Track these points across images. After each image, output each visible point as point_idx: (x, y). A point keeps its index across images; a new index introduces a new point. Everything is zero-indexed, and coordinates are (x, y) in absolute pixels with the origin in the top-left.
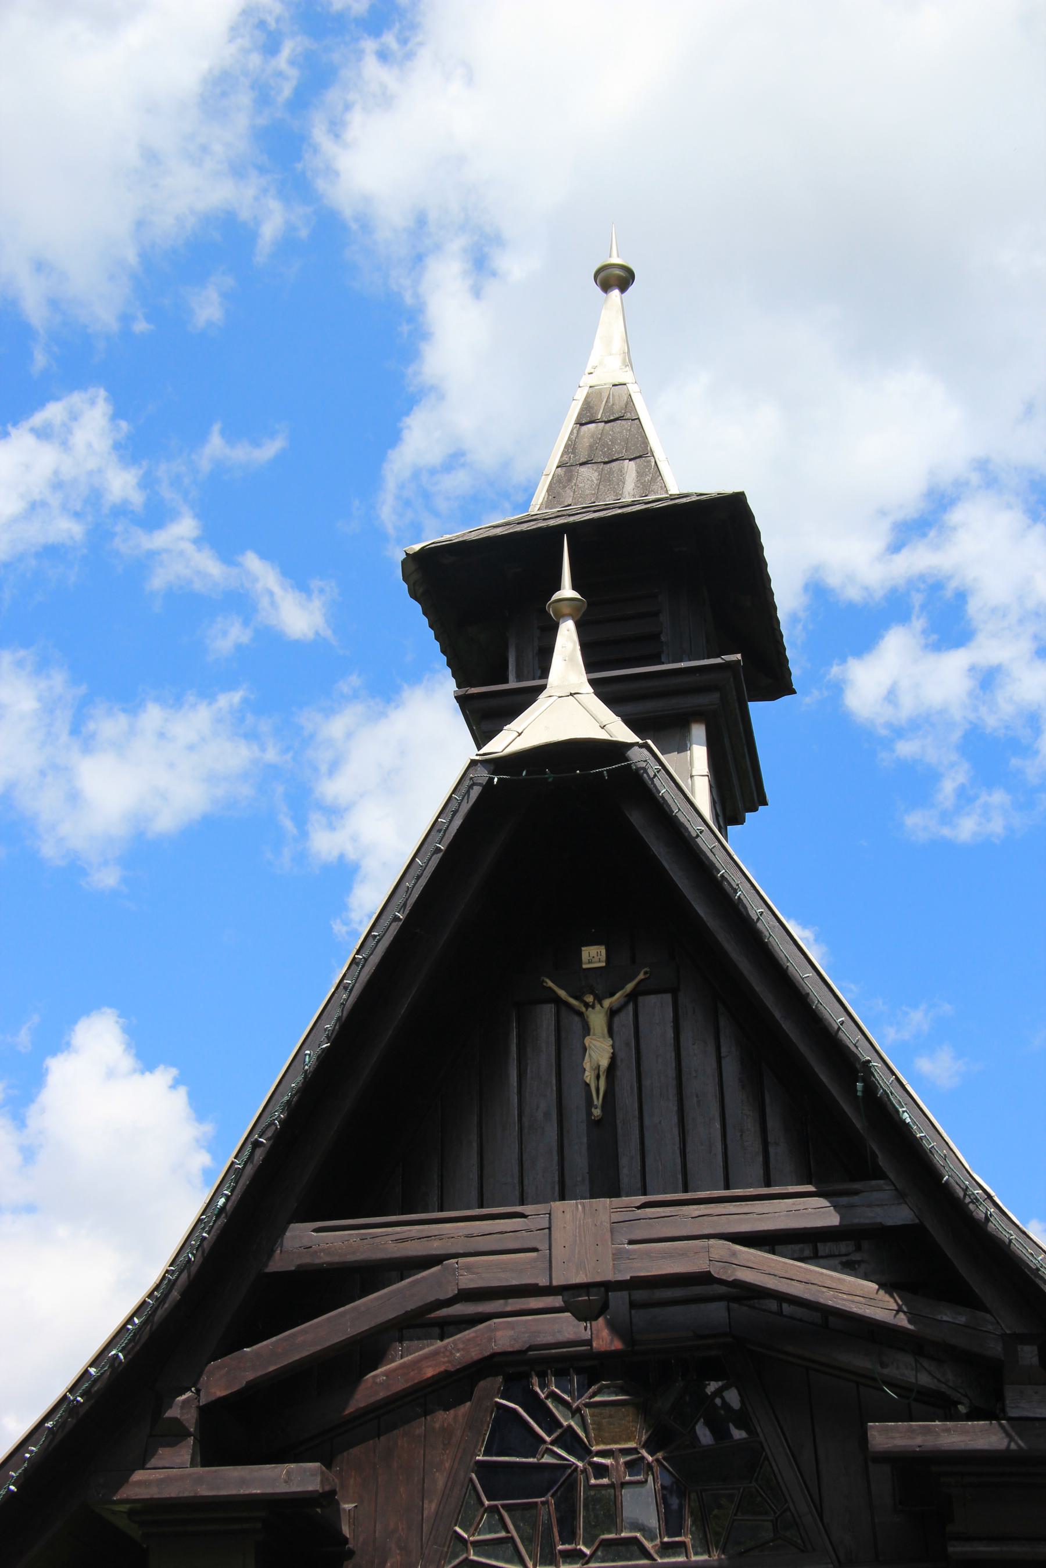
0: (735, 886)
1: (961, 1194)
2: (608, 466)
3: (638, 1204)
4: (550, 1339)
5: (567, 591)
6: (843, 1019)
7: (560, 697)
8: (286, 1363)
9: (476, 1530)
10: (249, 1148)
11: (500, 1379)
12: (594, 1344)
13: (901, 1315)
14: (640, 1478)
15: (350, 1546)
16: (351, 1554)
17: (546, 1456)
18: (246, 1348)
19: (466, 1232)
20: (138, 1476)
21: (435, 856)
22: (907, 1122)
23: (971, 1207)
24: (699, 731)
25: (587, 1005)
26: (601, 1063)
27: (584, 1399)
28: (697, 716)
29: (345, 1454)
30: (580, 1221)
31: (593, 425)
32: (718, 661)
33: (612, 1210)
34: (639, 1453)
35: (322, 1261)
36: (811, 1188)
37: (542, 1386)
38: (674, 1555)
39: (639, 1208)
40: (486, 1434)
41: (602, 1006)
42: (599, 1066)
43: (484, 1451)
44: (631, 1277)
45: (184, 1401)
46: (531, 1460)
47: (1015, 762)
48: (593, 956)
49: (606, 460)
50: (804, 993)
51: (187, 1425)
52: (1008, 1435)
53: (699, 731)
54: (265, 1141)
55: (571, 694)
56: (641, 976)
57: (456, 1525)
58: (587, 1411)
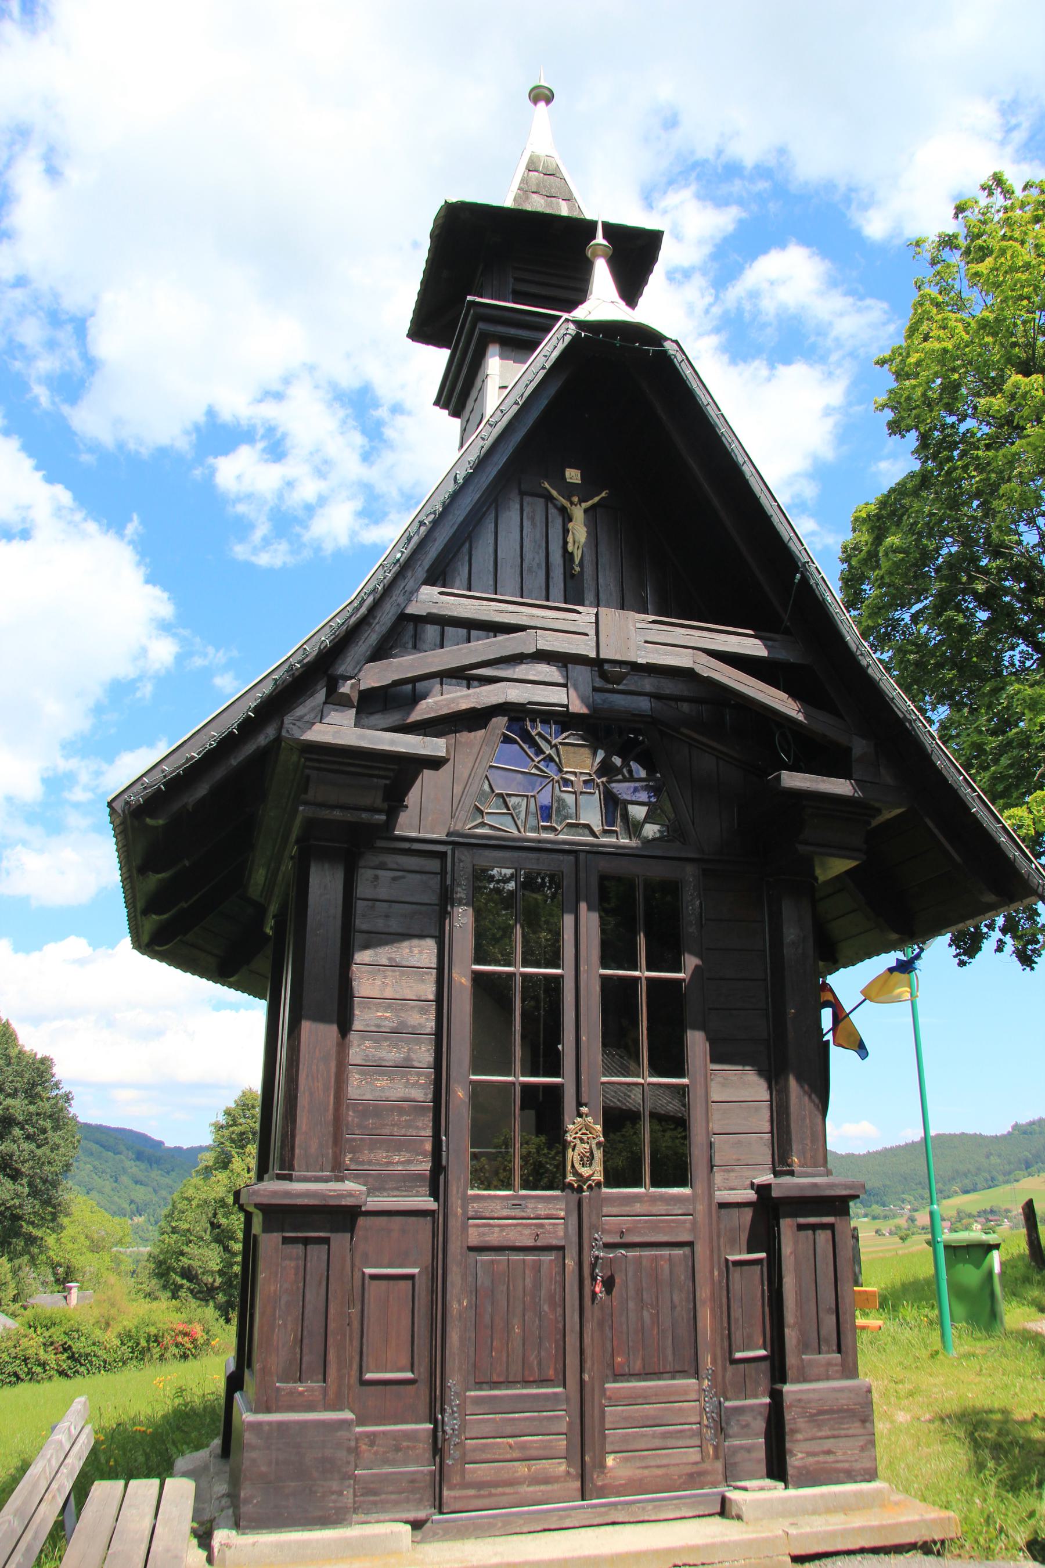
0: (730, 441)
10: (416, 524)
11: (506, 718)
12: (570, 707)
13: (800, 714)
14: (592, 791)
23: (860, 657)
25: (572, 503)
27: (559, 740)
36: (751, 632)
38: (610, 837)
39: (650, 622)
47: (298, 529)
48: (573, 475)
52: (854, 788)
55: (613, 302)
58: (560, 747)
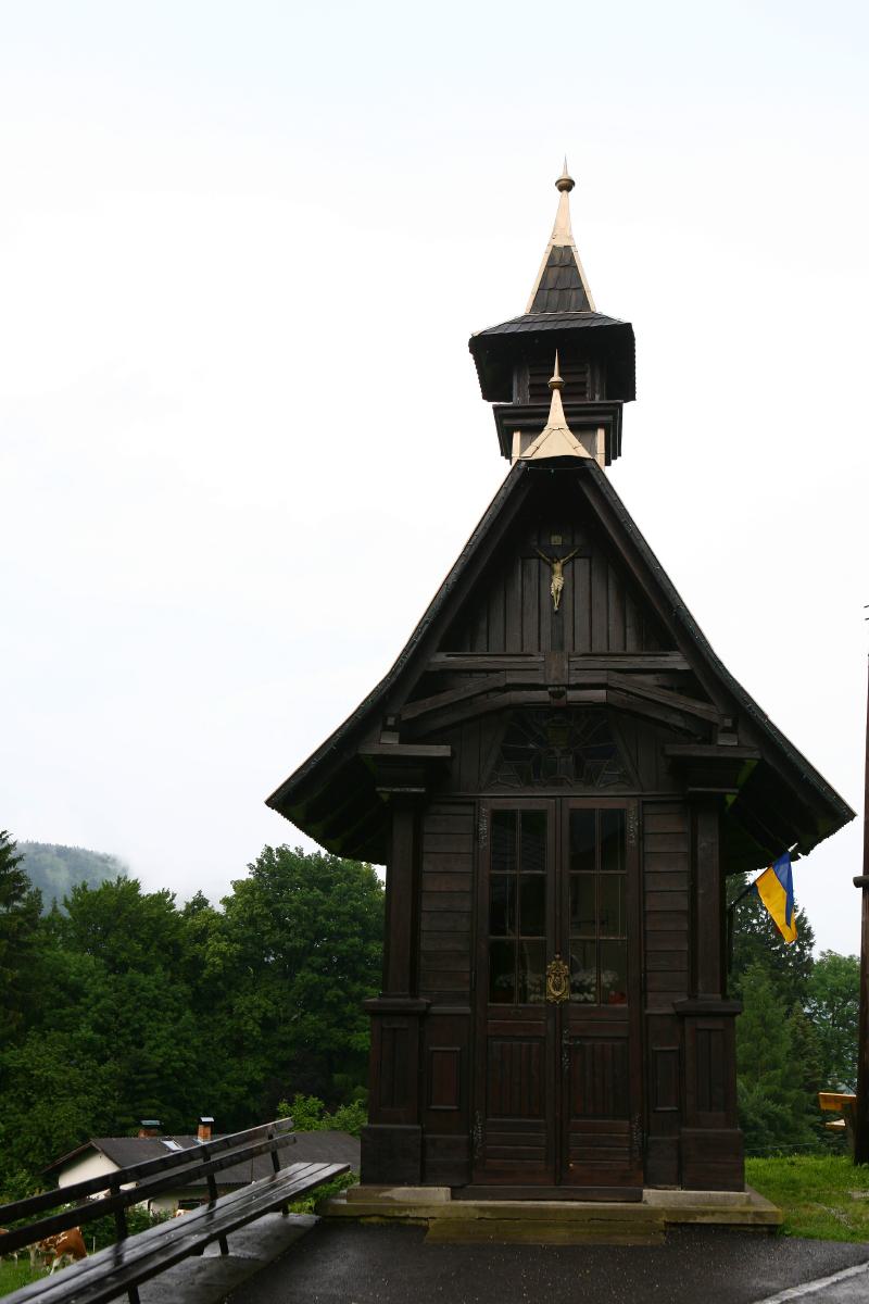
5: (556, 378)
28: (602, 425)
48: (556, 540)
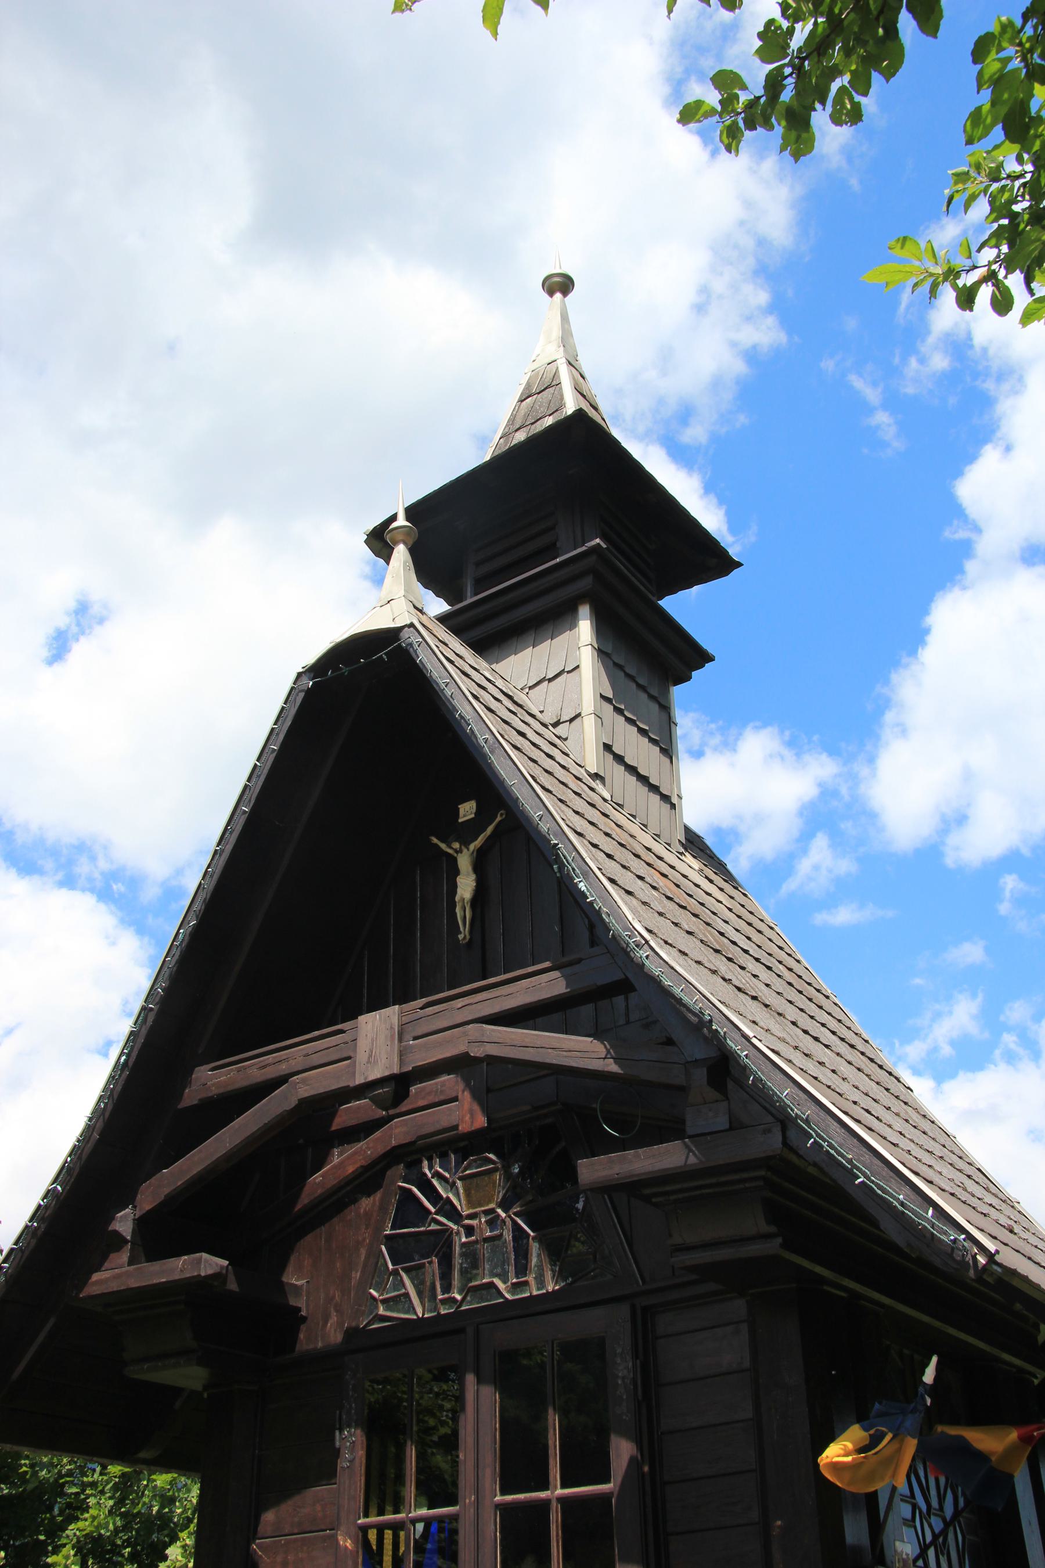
1: (625, 946)
2: (534, 425)
3: (421, 1006)
4: (432, 1129)
6: (541, 813)
7: (381, 607)
8: (188, 1177)
9: (384, 1290)
15: (303, 1313)
16: (304, 1319)
17: (432, 1224)
18: (165, 1169)
19: (305, 1052)
20: (96, 1277)
21: (271, 755)
22: (582, 890)
24: (584, 611)
26: (465, 897)
29: (302, 1241)
30: (377, 1028)
31: (530, 398)
32: (584, 548)
33: (402, 1015)
34: (496, 1212)
35: (213, 1093)
37: (430, 1168)
39: (421, 1009)
40: (392, 1213)
41: (468, 850)
42: (464, 899)
43: (391, 1226)
44: (413, 1068)
45: (121, 1217)
46: (422, 1229)
49: (533, 421)
50: (515, 797)
51: (124, 1234)
53: (584, 611)
54: (153, 1007)
56: (499, 819)
57: (370, 1289)
